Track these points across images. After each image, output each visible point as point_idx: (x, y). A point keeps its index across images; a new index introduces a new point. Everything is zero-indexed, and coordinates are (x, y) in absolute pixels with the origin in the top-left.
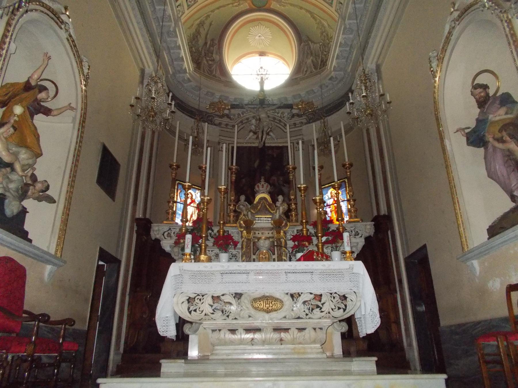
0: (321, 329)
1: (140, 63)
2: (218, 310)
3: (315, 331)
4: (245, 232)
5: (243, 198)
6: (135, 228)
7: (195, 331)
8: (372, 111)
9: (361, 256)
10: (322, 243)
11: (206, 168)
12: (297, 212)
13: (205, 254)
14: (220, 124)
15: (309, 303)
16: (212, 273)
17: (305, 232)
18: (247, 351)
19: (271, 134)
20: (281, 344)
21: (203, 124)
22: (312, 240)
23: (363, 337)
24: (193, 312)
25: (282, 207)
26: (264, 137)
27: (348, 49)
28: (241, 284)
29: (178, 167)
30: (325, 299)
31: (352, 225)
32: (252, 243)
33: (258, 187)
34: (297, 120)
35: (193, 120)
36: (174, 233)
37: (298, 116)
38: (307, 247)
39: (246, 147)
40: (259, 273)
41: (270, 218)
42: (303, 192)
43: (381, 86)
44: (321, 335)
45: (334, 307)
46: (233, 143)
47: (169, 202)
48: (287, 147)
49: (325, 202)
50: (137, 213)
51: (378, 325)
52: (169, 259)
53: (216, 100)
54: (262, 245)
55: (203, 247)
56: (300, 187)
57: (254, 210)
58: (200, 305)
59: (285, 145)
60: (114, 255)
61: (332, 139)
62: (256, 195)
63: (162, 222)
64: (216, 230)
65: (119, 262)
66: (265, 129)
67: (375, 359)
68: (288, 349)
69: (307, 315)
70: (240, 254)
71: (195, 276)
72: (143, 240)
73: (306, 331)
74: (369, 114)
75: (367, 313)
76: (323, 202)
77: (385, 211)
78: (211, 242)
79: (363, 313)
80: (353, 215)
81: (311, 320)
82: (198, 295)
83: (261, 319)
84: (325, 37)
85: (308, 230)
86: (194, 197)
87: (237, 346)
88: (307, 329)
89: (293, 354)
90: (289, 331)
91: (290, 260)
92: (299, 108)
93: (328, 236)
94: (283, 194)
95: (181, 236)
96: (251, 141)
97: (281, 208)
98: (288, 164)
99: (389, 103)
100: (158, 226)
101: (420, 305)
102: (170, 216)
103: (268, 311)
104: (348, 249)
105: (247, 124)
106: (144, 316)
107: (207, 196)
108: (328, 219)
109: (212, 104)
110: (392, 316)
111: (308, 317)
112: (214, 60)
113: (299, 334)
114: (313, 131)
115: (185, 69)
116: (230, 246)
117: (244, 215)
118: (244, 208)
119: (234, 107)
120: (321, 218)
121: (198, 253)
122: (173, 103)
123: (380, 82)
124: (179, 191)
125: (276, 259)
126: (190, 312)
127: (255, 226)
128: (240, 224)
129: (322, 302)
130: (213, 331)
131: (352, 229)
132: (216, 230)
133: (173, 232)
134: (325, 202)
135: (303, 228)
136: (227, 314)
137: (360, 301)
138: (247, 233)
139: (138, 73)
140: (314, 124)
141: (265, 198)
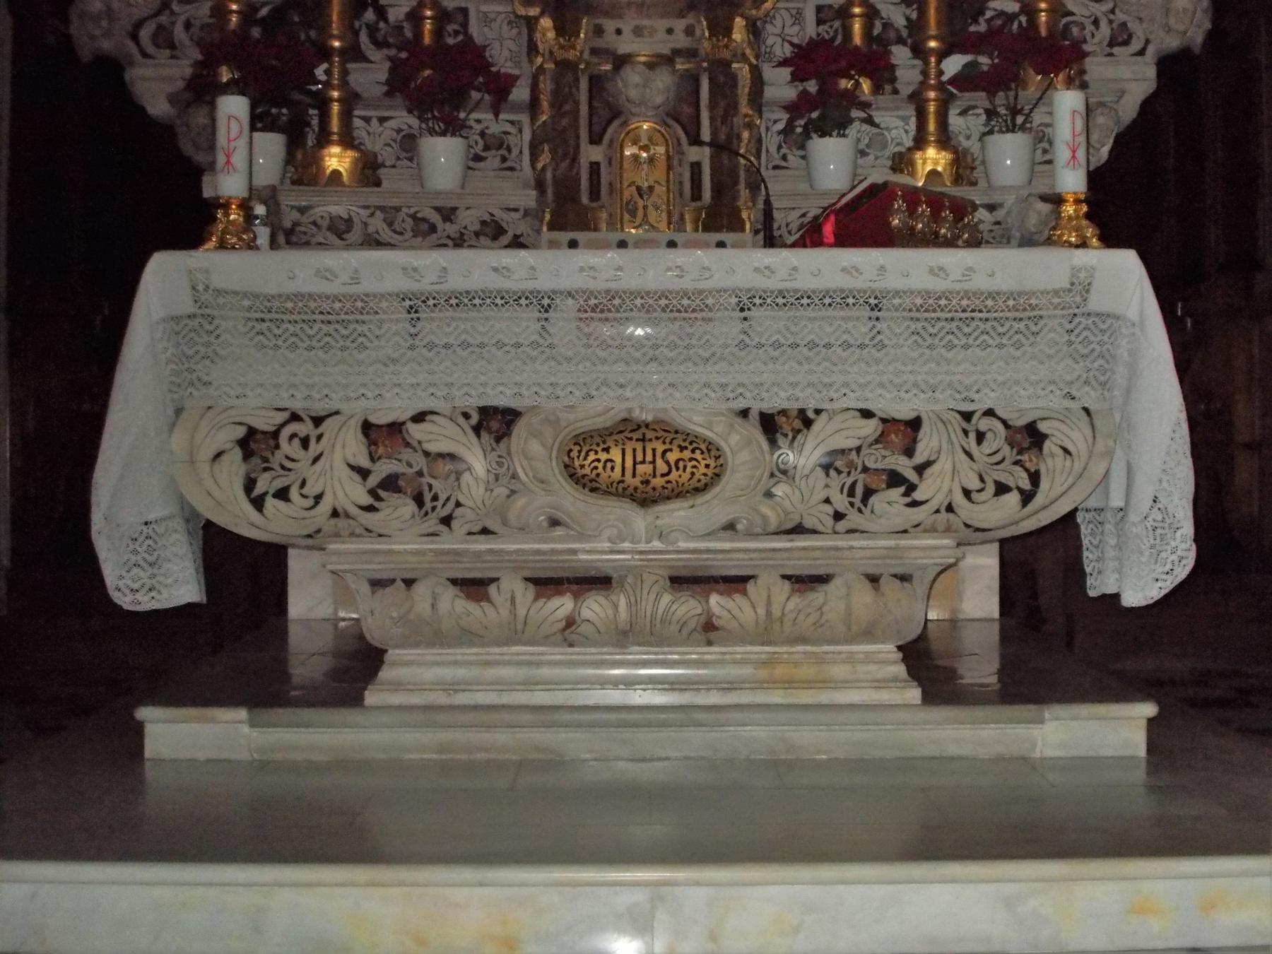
0: (904, 578)
2: (398, 490)
3: (877, 589)
4: (546, 22)
13: (348, 141)
15: (851, 465)
18: (545, 672)
20: (710, 643)
24: (270, 502)
30: (934, 444)
32: (584, 84)
38: (865, 106)
40: (604, 306)
45: (974, 484)
51: (1182, 572)
54: (633, 94)
55: (336, 107)
58: (303, 466)
67: (1149, 709)
69: (838, 516)
70: (527, 135)
78: (371, 76)
81: (858, 542)
82: (295, 417)
83: (607, 533)
87: (496, 650)
88: (837, 582)
89: (759, 685)
90: (750, 587)
93: (979, 53)
103: (645, 498)
111: (842, 526)
113: (795, 601)
116: (475, 95)
126: (258, 503)
129: (919, 458)
136: (445, 512)
137: (1109, 454)
138: (560, 30)
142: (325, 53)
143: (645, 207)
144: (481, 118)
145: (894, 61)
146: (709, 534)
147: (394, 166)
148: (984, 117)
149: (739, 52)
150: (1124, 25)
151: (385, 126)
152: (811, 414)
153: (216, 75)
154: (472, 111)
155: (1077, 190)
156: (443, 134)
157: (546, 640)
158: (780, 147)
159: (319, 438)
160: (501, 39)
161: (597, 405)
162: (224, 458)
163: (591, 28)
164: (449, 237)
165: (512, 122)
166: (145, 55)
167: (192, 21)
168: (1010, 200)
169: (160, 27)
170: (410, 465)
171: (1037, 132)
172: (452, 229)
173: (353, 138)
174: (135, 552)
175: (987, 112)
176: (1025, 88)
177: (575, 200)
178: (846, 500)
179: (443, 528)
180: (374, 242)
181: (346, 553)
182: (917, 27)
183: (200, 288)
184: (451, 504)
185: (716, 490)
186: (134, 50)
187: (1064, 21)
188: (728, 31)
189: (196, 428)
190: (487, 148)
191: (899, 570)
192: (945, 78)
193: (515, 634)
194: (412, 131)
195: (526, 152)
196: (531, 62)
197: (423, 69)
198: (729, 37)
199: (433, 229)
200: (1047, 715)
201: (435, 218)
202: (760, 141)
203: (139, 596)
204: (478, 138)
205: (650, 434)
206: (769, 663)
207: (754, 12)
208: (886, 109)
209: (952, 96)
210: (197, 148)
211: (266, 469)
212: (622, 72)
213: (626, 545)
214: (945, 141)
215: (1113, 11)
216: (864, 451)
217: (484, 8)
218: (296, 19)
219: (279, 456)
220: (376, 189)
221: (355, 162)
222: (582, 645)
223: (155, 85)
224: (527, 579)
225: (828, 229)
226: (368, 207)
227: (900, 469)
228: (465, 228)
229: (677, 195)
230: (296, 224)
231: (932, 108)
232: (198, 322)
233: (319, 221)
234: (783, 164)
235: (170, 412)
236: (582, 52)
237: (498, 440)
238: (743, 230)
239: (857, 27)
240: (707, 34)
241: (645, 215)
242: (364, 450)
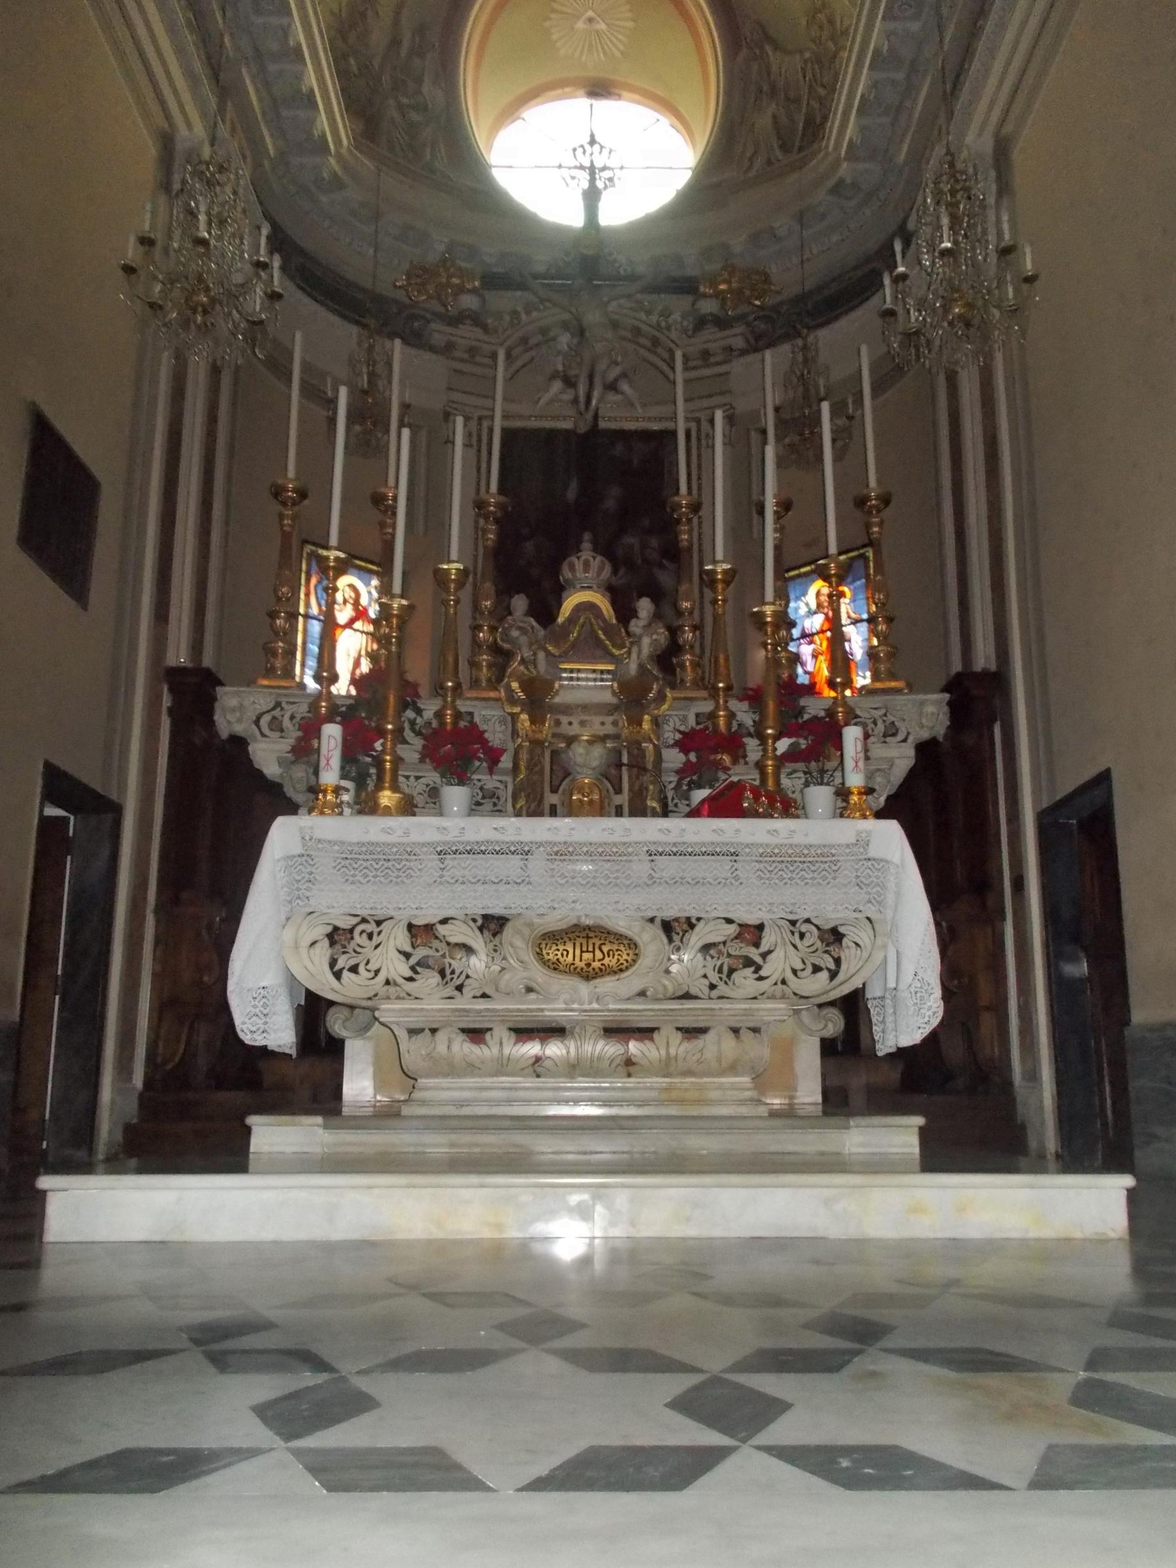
0: (755, 1030)
1: (154, 107)
2: (428, 967)
4: (524, 717)
5: (520, 603)
6: (167, 701)
7: (364, 1030)
8: (970, 306)
9: (897, 807)
10: (775, 758)
11: (395, 499)
13: (395, 788)
14: (450, 347)
15: (720, 953)
16: (410, 852)
17: (722, 722)
18: (521, 1094)
19: (625, 386)
20: (629, 1075)
21: (388, 343)
22: (739, 747)
23: (890, 1055)
24: (346, 974)
25: (648, 639)
26: (596, 394)
27: (900, 76)
28: (502, 888)
29: (303, 494)
30: (773, 939)
31: (878, 700)
32: (547, 754)
33: (572, 568)
34: (712, 339)
35: (354, 330)
36: (292, 718)
37: (722, 323)
40: (562, 853)
41: (608, 672)
43: (1005, 218)
44: (758, 1050)
46: (492, 418)
47: (273, 615)
48: (673, 434)
49: (793, 624)
51: (935, 1022)
52: (278, 801)
53: (432, 258)
54: (579, 760)
56: (714, 572)
57: (557, 646)
58: (368, 951)
59: (669, 425)
60: (99, 789)
61: (825, 407)
62: (564, 595)
63: (251, 682)
64: (430, 707)
65: (116, 810)
66: (601, 366)
67: (920, 1121)
68: (651, 1089)
71: (357, 860)
72: (197, 741)
73: (710, 1037)
74: (960, 317)
75: (902, 986)
76: (785, 622)
77: (987, 658)
78: (411, 750)
79: (891, 984)
80: (882, 667)
81: (725, 1005)
83: (563, 997)
84: (821, 28)
85: (731, 716)
86: (364, 601)
87: (489, 1080)
89: (660, 1103)
90: (656, 1035)
91: (665, 813)
92: (718, 295)
93: (797, 736)
94: (657, 595)
95: (310, 730)
96: (552, 410)
99: (1030, 280)
100: (237, 694)
101: (1074, 959)
102: (279, 663)
103: (588, 975)
104: (855, 780)
106: (206, 979)
107: (402, 597)
108: (803, 679)
109: (420, 274)
110: (985, 993)
111: (715, 993)
112: (426, 109)
113: (686, 1045)
114: (767, 376)
115: (323, 137)
116: (477, 763)
118: (523, 640)
119: (494, 281)
120: (779, 677)
121: (371, 786)
122: (276, 263)
123: (1005, 202)
124: (314, 581)
125: (626, 810)
126: (338, 975)
127: (557, 700)
128: (509, 690)
129: (764, 947)
130: (413, 1032)
132: (430, 707)
133: (287, 716)
134: (793, 624)
135: (717, 708)
136: (459, 982)
137: (885, 947)
138: (532, 722)
139: (153, 151)
140: (768, 355)
142: (382, 733)
146: (628, 999)
150: (893, 723)
152: (694, 921)
157: (520, 1072)
159: (379, 933)
160: (494, 732)
161: (557, 915)
162: (317, 945)
169: (274, 718)
170: (437, 951)
174: (255, 1007)
178: (717, 975)
179: (456, 993)
181: (393, 1010)
183: (307, 838)
184: (463, 977)
185: (634, 968)
189: (300, 926)
191: (751, 1025)
193: (503, 1067)
195: (510, 800)
196: (514, 742)
198: (641, 725)
200: (852, 1123)
203: (255, 1036)
205: (592, 934)
206: (668, 1089)
211: (344, 953)
213: (575, 1006)
215: (885, 715)
216: (728, 944)
218: (363, 715)
219: (353, 945)
222: (546, 1076)
224: (510, 1029)
227: (751, 956)
232: (303, 858)
235: (283, 918)
237: (494, 935)
242: (408, 941)
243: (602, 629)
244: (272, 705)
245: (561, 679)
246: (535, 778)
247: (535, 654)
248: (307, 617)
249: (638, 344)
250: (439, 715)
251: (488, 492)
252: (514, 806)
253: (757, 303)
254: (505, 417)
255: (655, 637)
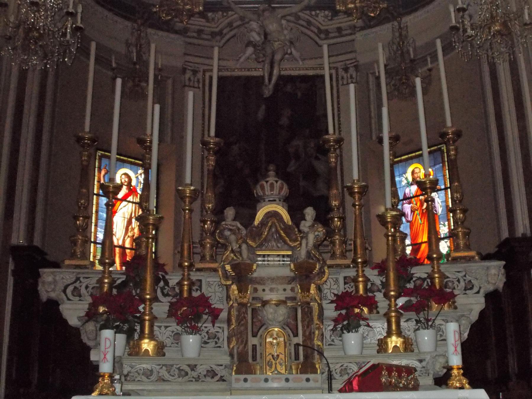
4: (234, 287)
5: (230, 212)
11: (151, 142)
12: (345, 236)
13: (152, 337)
36: (87, 287)
38: (365, 319)
39: (238, 78)
41: (288, 256)
42: (357, 196)
46: (211, 70)
47: (76, 218)
48: (322, 77)
50: (14, 235)
54: (270, 316)
55: (147, 323)
57: (254, 240)
59: (318, 72)
77: (525, 226)
78: (161, 308)
80: (461, 243)
86: (134, 183)
97: (311, 238)
98: (327, 133)
100: (52, 273)
102: (78, 250)
105: (242, 29)
116: (205, 317)
117: (233, 251)
118: (233, 238)
121: (136, 336)
124: (103, 173)
127: (255, 275)
131: (460, 275)
133: (84, 286)
138: (240, 291)
141: (274, 215)
142: (143, 301)
143: (276, 364)
144: (206, 325)
145: (376, 299)
147: (170, 347)
148: (415, 322)
149: (313, 299)
150: (470, 281)
151: (167, 330)
153: (97, 310)
154: (204, 323)
155: (458, 364)
156: (191, 334)
158: (331, 336)
163: (253, 289)
164: (193, 377)
165: (220, 327)
166: (69, 299)
167: (89, 286)
168: (428, 357)
171: (437, 328)
172: (195, 374)
173: (154, 336)
175: (416, 320)
176: (431, 310)
177: (247, 361)
180: (162, 380)
182: (385, 285)
186: (65, 297)
187: (445, 280)
188: (308, 290)
190: (209, 338)
192: (398, 307)
194: (178, 332)
195: (226, 339)
196: (228, 303)
197: (184, 307)
199: (187, 374)
201: (188, 369)
202: (322, 335)
204: (206, 334)
207: (319, 282)
208: (375, 320)
209: (401, 314)
210: (89, 339)
212: (265, 308)
214: (399, 334)
215: (465, 276)
217: (208, 280)
220: (163, 358)
221: (155, 346)
223: (73, 312)
225: (355, 384)
226: (160, 365)
228: (200, 373)
229: (289, 359)
230: (129, 372)
231: (393, 320)
233: (139, 371)
234: (332, 343)
236: (249, 299)
238: (317, 373)
239: (361, 286)
240: (300, 291)
241: (276, 367)
243: (282, 229)
244: (74, 279)
245: (257, 261)
246: (242, 328)
247: (240, 247)
248: (95, 243)
249: (299, 25)
250: (180, 284)
251: (209, 136)
252: (229, 347)
253: (372, 15)
254: (219, 70)
255: (316, 233)
